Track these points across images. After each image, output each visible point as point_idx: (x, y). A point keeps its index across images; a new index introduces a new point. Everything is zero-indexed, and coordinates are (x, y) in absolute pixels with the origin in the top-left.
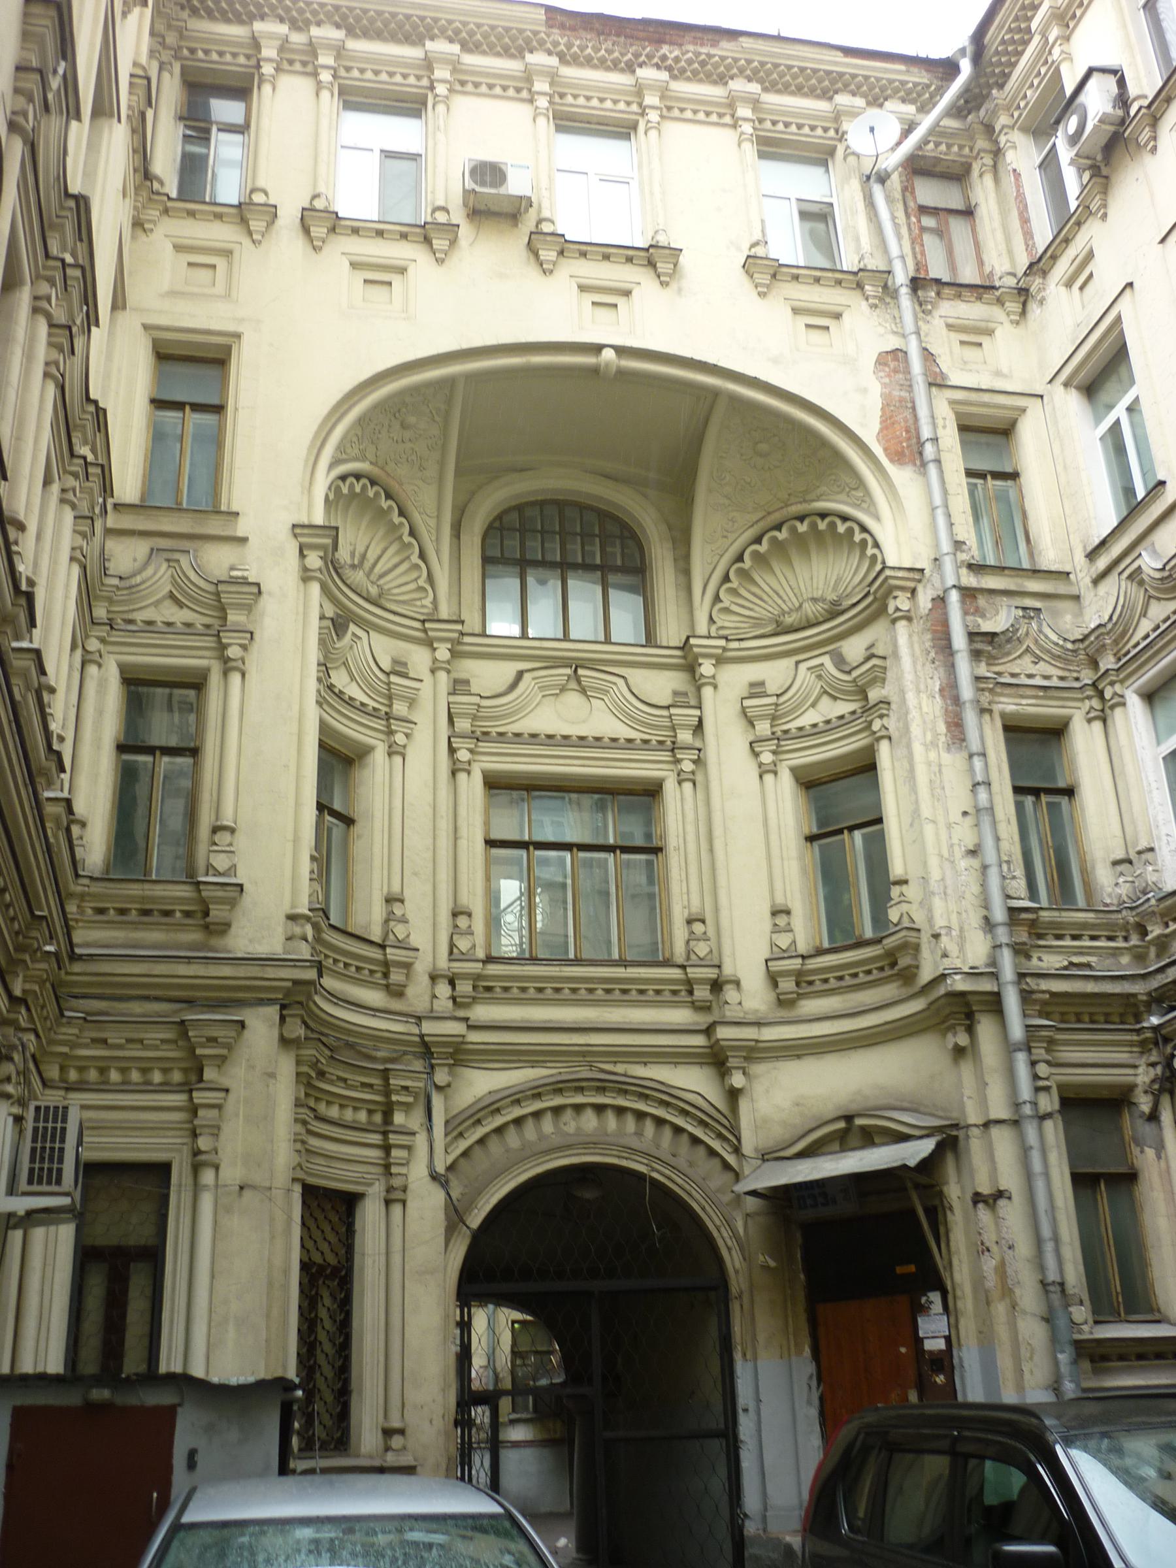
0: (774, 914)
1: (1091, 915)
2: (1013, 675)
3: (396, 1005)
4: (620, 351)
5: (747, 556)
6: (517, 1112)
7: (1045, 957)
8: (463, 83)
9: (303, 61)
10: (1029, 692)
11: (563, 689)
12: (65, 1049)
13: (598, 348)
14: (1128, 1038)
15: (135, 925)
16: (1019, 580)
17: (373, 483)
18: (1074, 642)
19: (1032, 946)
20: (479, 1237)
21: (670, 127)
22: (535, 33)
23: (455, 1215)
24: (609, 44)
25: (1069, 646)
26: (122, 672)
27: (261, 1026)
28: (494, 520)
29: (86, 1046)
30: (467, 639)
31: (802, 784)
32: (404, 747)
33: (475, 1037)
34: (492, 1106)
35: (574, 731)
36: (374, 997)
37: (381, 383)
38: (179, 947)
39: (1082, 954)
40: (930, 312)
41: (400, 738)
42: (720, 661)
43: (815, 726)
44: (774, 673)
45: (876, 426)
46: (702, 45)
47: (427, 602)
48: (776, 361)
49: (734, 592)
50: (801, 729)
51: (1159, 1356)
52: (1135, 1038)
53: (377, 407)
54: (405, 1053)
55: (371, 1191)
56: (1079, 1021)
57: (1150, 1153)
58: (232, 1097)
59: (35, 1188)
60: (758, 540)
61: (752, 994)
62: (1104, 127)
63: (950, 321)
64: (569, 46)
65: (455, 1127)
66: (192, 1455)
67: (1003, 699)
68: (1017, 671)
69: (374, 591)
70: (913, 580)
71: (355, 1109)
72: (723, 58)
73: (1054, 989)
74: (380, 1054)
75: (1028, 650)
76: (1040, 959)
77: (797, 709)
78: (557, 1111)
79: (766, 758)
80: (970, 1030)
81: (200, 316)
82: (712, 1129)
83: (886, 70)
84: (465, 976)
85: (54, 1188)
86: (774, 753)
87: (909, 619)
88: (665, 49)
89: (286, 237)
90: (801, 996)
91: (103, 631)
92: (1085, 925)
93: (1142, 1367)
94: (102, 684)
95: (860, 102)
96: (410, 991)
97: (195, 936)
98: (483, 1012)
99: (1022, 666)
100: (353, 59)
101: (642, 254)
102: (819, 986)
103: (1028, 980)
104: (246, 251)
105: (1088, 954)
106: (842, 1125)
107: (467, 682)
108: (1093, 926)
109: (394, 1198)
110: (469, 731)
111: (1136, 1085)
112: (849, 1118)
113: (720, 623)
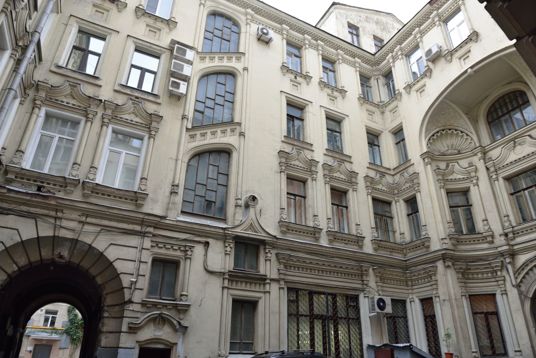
4: (471, 67)
8: (423, 33)
9: (395, 59)
13: (466, 71)
15: (415, 251)
17: (443, 130)
27: (440, 265)
30: (486, 148)
33: (515, 247)
34: (525, 264)
36: (486, 246)
37: (176, 287)
41: (475, 181)
47: (473, 145)
53: (430, 117)
55: (497, 292)
58: (438, 281)
69: (456, 152)
71: (487, 274)
94: (400, 205)
96: (495, 241)
97: (425, 249)
98: (519, 240)
107: (491, 158)
109: (505, 293)
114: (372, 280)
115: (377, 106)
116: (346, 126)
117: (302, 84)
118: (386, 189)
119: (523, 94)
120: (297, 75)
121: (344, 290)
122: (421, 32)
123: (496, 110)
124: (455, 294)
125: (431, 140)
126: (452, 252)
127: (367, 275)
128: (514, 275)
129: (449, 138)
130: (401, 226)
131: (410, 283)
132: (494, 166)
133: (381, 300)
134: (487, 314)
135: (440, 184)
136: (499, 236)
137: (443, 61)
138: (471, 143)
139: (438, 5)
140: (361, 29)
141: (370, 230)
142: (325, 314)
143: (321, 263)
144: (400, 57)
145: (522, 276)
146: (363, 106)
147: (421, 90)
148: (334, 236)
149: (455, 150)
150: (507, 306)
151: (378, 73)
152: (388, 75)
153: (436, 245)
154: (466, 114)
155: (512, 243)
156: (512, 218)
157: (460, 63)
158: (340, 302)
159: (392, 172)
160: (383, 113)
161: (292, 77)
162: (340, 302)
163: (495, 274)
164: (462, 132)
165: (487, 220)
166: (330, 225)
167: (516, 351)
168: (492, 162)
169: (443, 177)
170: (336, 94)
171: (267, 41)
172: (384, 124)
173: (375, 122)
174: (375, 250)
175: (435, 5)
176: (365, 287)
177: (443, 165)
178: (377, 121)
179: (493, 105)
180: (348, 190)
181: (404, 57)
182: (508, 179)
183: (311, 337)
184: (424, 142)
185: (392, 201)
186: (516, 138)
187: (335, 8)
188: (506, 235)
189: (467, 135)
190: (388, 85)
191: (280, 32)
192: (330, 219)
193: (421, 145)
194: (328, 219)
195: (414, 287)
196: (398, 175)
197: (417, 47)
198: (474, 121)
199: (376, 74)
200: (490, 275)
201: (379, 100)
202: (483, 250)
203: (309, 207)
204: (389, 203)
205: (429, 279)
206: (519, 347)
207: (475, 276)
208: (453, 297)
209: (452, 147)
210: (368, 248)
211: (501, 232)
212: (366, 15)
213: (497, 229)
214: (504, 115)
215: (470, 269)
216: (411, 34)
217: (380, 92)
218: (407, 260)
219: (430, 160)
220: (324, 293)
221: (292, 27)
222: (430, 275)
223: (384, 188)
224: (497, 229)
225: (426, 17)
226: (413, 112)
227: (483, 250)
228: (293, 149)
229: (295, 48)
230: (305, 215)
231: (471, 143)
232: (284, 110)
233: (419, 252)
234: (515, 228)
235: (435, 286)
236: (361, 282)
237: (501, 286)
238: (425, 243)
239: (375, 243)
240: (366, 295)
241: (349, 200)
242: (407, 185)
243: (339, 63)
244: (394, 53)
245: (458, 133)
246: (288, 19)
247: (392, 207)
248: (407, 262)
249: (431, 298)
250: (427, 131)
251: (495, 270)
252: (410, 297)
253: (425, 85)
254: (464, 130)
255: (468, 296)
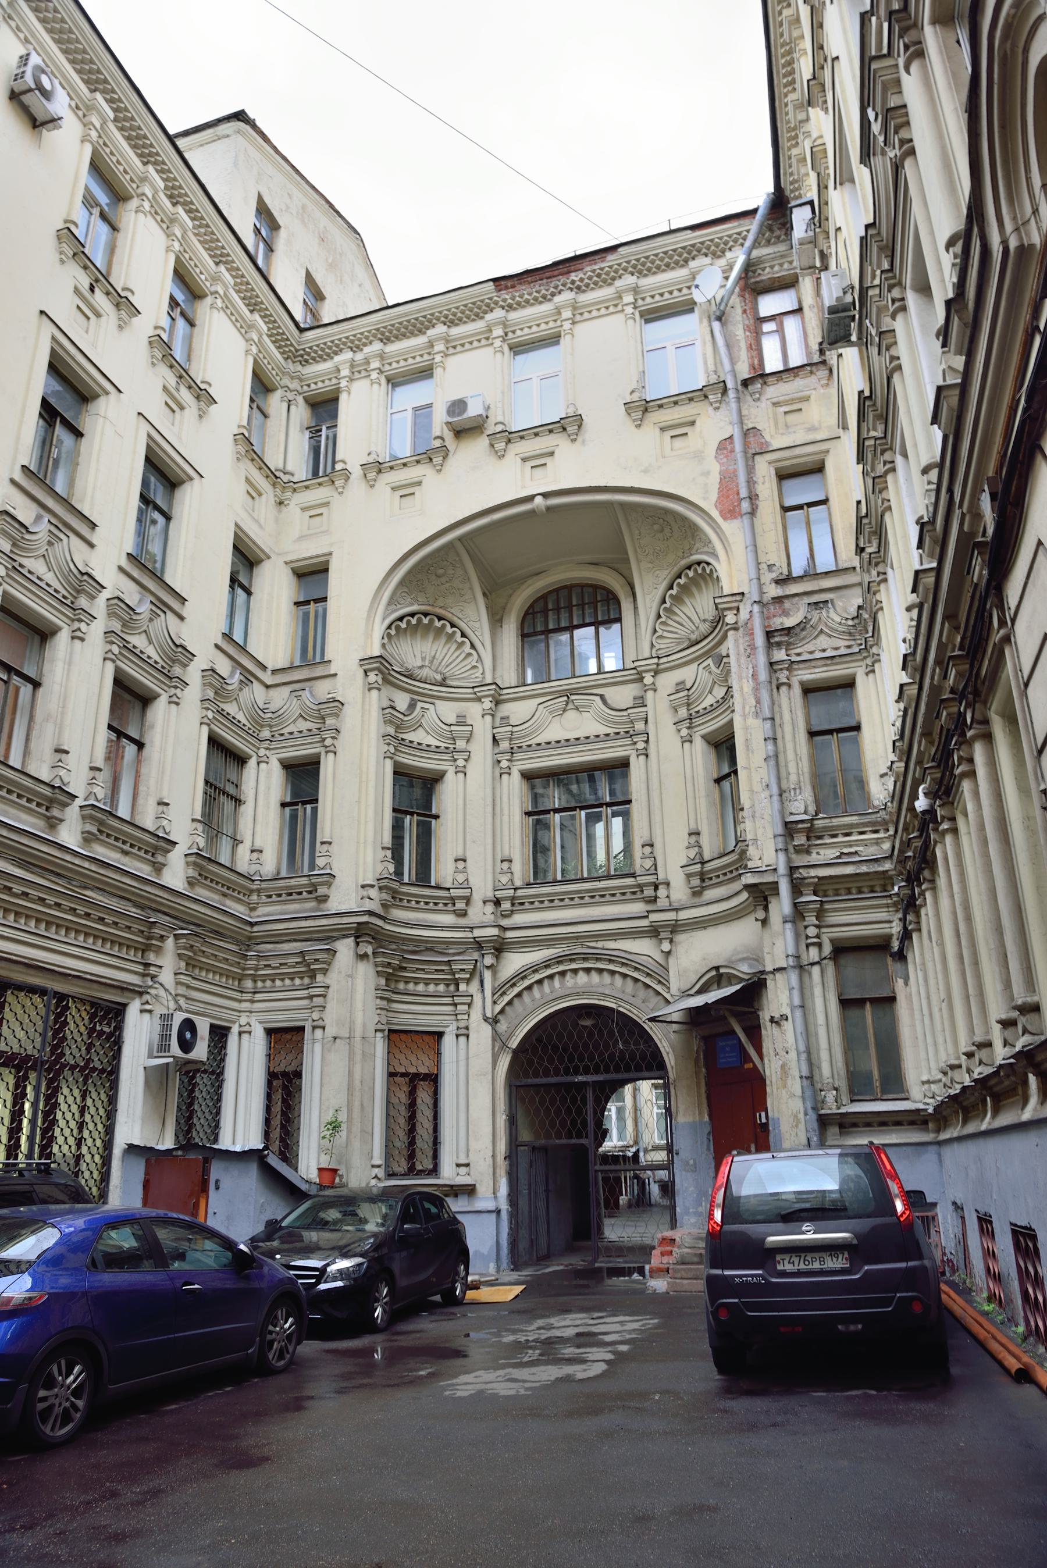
0: (690, 834)
1: (856, 818)
2: (811, 653)
3: (462, 922)
4: (545, 495)
5: (667, 599)
6: (537, 977)
7: (822, 852)
8: (453, 346)
9: (358, 371)
10: (819, 663)
11: (564, 710)
12: (252, 972)
13: (530, 498)
14: (885, 902)
16: (816, 582)
17: (426, 615)
18: (853, 619)
19: (809, 846)
20: (517, 1053)
21: (578, 328)
22: (491, 299)
23: (499, 1040)
24: (537, 288)
25: (850, 623)
26: (281, 763)
27: (345, 948)
28: (529, 608)
29: (262, 969)
30: (505, 692)
31: (709, 743)
32: (465, 767)
33: (510, 934)
34: (521, 975)
35: (572, 735)
36: (448, 919)
38: (305, 911)
39: (851, 846)
40: (759, 399)
41: (461, 763)
42: (656, 672)
43: (712, 705)
44: (687, 674)
45: (714, 496)
46: (595, 264)
47: (479, 674)
48: (645, 471)
49: (664, 623)
50: (705, 709)
51: (898, 1123)
52: (889, 901)
53: (410, 572)
54: (468, 949)
55: (447, 1030)
56: (872, 891)
57: (900, 982)
58: (331, 989)
59: (160, 1054)
60: (671, 588)
61: (679, 891)
62: (804, 247)
63: (775, 400)
64: (513, 298)
65: (499, 991)
66: (217, 1181)
67: (800, 672)
68: (813, 649)
69: (439, 677)
70: (736, 601)
71: (437, 985)
72: (610, 267)
73: (821, 875)
74: (451, 951)
75: (822, 631)
76: (818, 853)
77: (701, 697)
78: (563, 974)
79: (684, 732)
80: (766, 908)
81: (308, 551)
82: (655, 978)
83: (715, 233)
84: (506, 899)
85: (167, 1054)
86: (689, 728)
87: (736, 629)
88: (573, 276)
89: (356, 485)
90: (703, 888)
91: (265, 744)
92: (852, 826)
93: (880, 1131)
95: (707, 260)
96: (470, 912)
97: (313, 904)
98: (519, 919)
99: (805, 649)
100: (392, 357)
101: (558, 425)
102: (715, 880)
103: (801, 870)
104: (336, 500)
105: (857, 845)
106: (714, 973)
107: (507, 718)
108: (858, 825)
109: (464, 1033)
110: (507, 745)
111: (892, 935)
112: (717, 968)
113: (658, 646)
114: (168, 963)
115: (272, 476)
116: (189, 502)
117: (104, 319)
118: (244, 721)
119: (611, 599)
120: (97, 281)
121: (95, 986)
122: (448, 341)
123: (545, 612)
124: (364, 1025)
125: (401, 627)
126: (380, 923)
127: (158, 950)
128: (493, 994)
129: (431, 638)
130: (258, 828)
131: (248, 984)
132: (511, 739)
133: (189, 1025)
134: (414, 1080)
135: (386, 747)
136: (481, 903)
137: (482, 443)
138: (474, 667)
139: (513, 298)
140: (283, 233)
141: (189, 826)
142: (35, 1053)
143: (51, 899)
144: (374, 375)
145: (507, 999)
146: (241, 464)
147: (406, 491)
148: (103, 822)
149: (436, 671)
150: (462, 1064)
151: (294, 385)
152: (324, 407)
153: (346, 897)
154: (484, 594)
155: (505, 923)
156: (517, 867)
157: (522, 471)
158: (77, 1022)
159: (269, 679)
160: (281, 503)
161: (85, 282)
162: (77, 1022)
163: (452, 988)
164: (463, 635)
165: (465, 861)
166: (97, 790)
167: (458, 1165)
168: (509, 728)
169: (397, 726)
170: (185, 396)
171: (40, 117)
172: (286, 539)
173: (257, 521)
174: (189, 883)
175: (505, 295)
176: (150, 983)
177: (402, 701)
178: (262, 522)
179: (544, 598)
180: (157, 696)
181: (383, 381)
182: (528, 776)
183: (12, 1122)
184: (379, 629)
185: (250, 757)
186: (573, 692)
187: (239, 132)
188: (497, 902)
189: (473, 646)
190: (315, 432)
191: (82, 110)
192: (100, 770)
193: (368, 635)
194: (92, 769)
195: (258, 996)
196: (285, 691)
197: (425, 373)
198: (496, 619)
199: (291, 386)
200: (441, 988)
201: (281, 466)
202: (442, 928)
203: (47, 719)
204: (241, 760)
205: (307, 981)
206: (468, 1156)
207: (411, 986)
208: (358, 1033)
209: (431, 662)
210: (175, 874)
211: (490, 894)
212: (306, 201)
213: (482, 886)
214: (559, 630)
215: (405, 968)
216: (421, 332)
217: (288, 444)
218: (256, 923)
219: (380, 679)
220: (43, 992)
221: (123, 120)
222: (311, 970)
223: (240, 717)
224: (482, 886)
225: (477, 311)
226: (371, 538)
227: (442, 928)
228: (38, 518)
229: (110, 189)
230: (28, 740)
231: (474, 667)
232: (37, 383)
233: (293, 908)
234: (520, 893)
235: (317, 1001)
236: (140, 969)
237: (459, 1017)
238: (316, 888)
239: (195, 864)
240: (148, 1007)
241: (152, 727)
242: (304, 726)
243: (212, 306)
244: (359, 357)
245: (454, 633)
246: (119, 85)
247: (246, 772)
248: (255, 929)
249: (302, 1029)
250: (390, 603)
251: (456, 979)
252: (243, 1020)
253: (419, 483)
254: (468, 632)
255: (386, 1033)
